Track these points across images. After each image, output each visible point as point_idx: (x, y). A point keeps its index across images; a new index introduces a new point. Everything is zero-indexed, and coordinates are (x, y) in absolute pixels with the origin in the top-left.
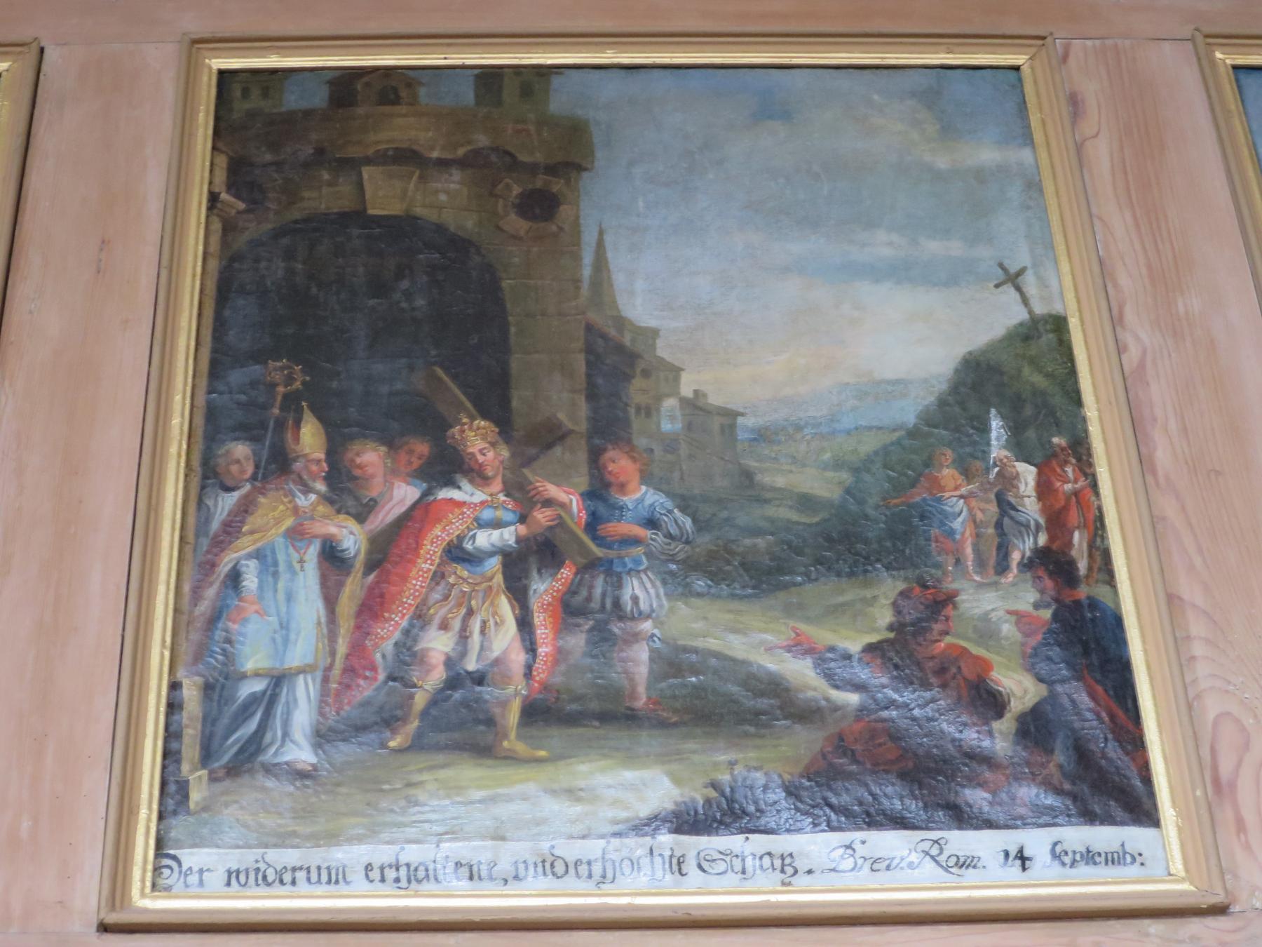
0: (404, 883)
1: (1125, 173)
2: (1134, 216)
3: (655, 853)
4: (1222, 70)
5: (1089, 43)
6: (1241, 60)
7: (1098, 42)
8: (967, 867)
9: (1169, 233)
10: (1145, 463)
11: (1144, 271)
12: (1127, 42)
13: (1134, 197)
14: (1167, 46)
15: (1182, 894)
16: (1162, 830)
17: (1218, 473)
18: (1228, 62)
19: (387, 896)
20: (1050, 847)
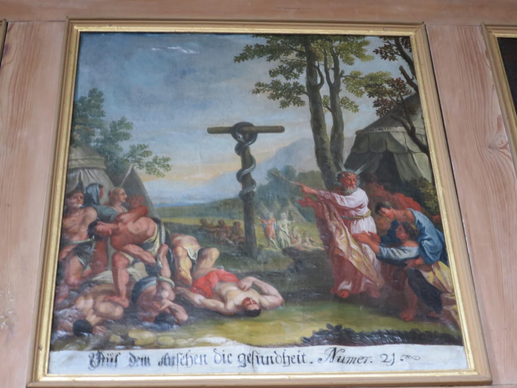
0: (287, 364)
1: (16, 78)
2: (13, 97)
3: (188, 356)
4: (75, 33)
5: (22, 23)
6: (84, 29)
7: (26, 23)
8: (350, 363)
9: (25, 103)
10: (512, 172)
11: (9, 120)
12: (38, 23)
13: (16, 87)
14: (55, 24)
15: (473, 376)
16: (464, 346)
17: (9, 205)
18: (79, 30)
19: (87, 376)
20: (387, 354)
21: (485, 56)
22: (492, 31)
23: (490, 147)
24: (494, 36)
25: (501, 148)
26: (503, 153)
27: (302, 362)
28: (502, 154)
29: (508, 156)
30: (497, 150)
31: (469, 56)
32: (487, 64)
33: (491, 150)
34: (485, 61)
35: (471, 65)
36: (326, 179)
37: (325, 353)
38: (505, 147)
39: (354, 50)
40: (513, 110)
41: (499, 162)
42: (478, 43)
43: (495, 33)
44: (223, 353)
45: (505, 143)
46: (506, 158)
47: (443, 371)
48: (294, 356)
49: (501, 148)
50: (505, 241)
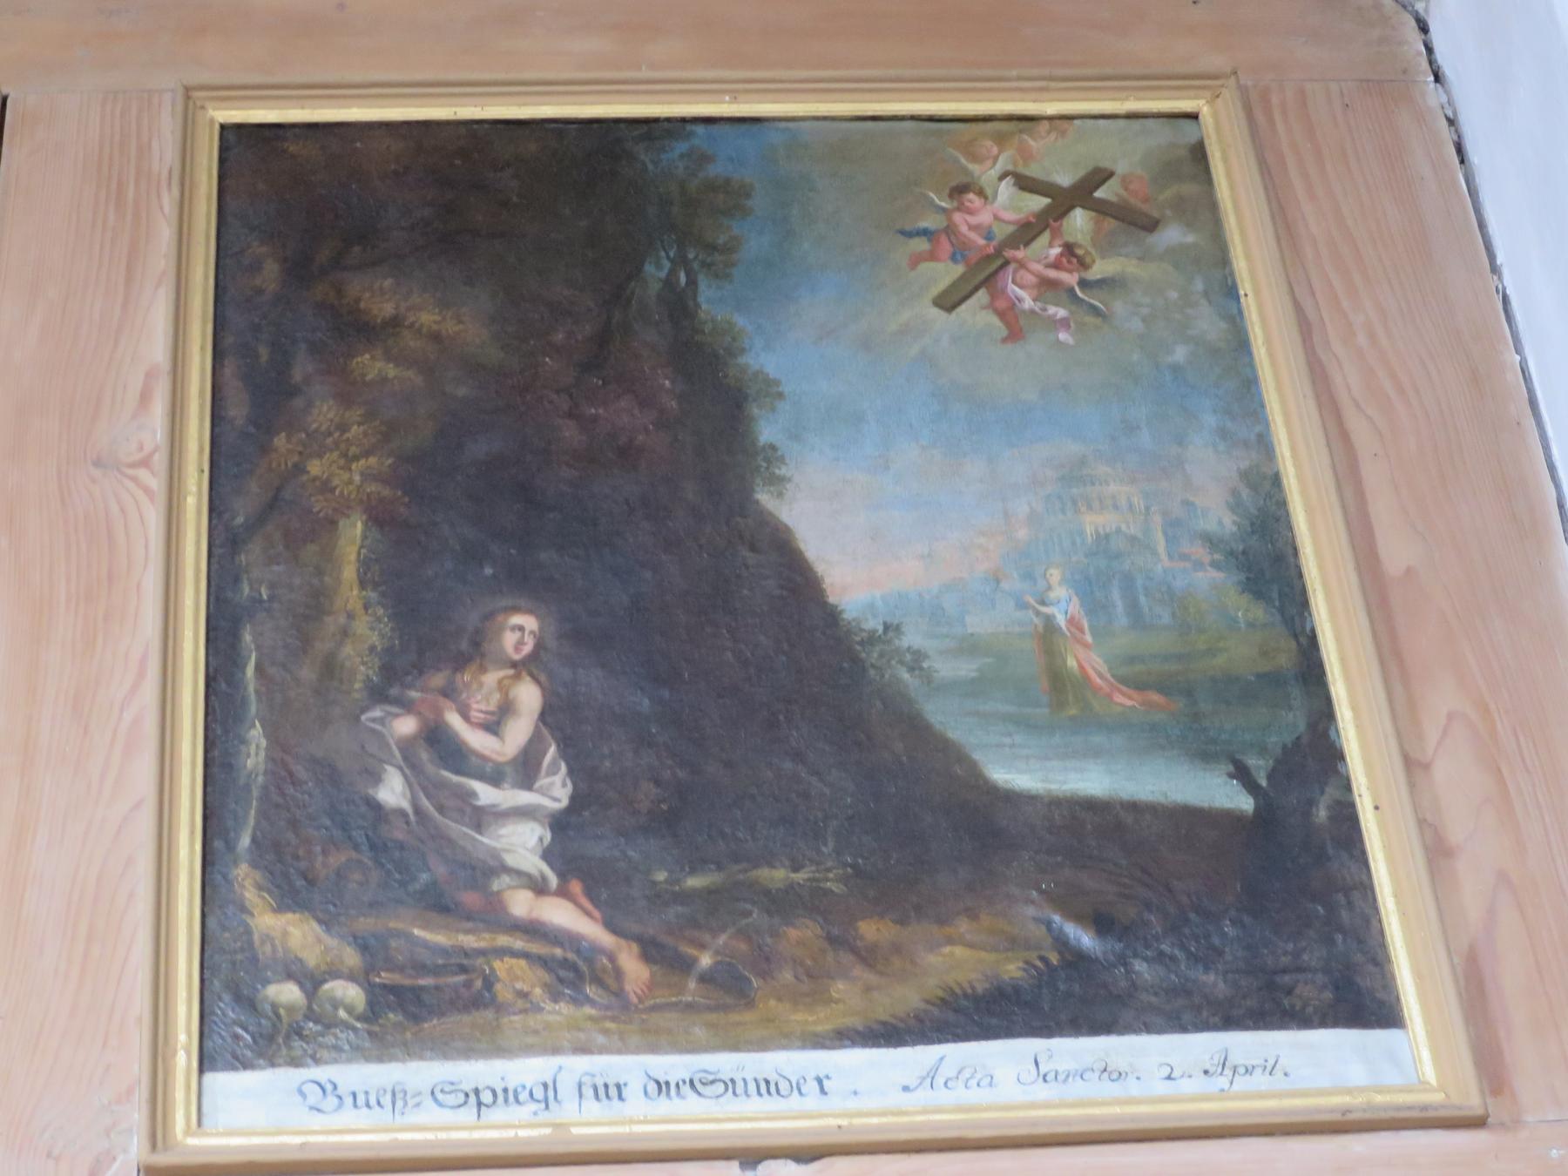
21: (164, 183)
22: (209, 105)
23: (97, 463)
24: (212, 121)
25: (133, 465)
26: (134, 479)
27: (377, 1106)
28: (130, 485)
29: (147, 491)
30: (118, 470)
31: (114, 186)
32: (161, 208)
33: (96, 472)
34: (159, 196)
35: (112, 217)
36: (981, 782)
37: (1172, 1069)
38: (145, 463)
39: (367, 359)
40: (203, 348)
41: (115, 509)
42: (155, 144)
43: (214, 109)
44: (503, 1085)
45: (148, 447)
46: (140, 494)
47: (632, 1122)
48: (385, 1091)
49: (133, 465)
50: (67, 749)
